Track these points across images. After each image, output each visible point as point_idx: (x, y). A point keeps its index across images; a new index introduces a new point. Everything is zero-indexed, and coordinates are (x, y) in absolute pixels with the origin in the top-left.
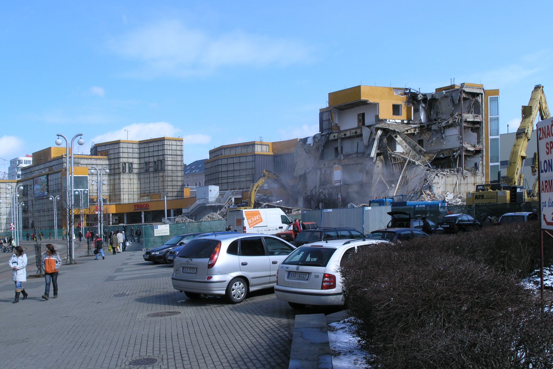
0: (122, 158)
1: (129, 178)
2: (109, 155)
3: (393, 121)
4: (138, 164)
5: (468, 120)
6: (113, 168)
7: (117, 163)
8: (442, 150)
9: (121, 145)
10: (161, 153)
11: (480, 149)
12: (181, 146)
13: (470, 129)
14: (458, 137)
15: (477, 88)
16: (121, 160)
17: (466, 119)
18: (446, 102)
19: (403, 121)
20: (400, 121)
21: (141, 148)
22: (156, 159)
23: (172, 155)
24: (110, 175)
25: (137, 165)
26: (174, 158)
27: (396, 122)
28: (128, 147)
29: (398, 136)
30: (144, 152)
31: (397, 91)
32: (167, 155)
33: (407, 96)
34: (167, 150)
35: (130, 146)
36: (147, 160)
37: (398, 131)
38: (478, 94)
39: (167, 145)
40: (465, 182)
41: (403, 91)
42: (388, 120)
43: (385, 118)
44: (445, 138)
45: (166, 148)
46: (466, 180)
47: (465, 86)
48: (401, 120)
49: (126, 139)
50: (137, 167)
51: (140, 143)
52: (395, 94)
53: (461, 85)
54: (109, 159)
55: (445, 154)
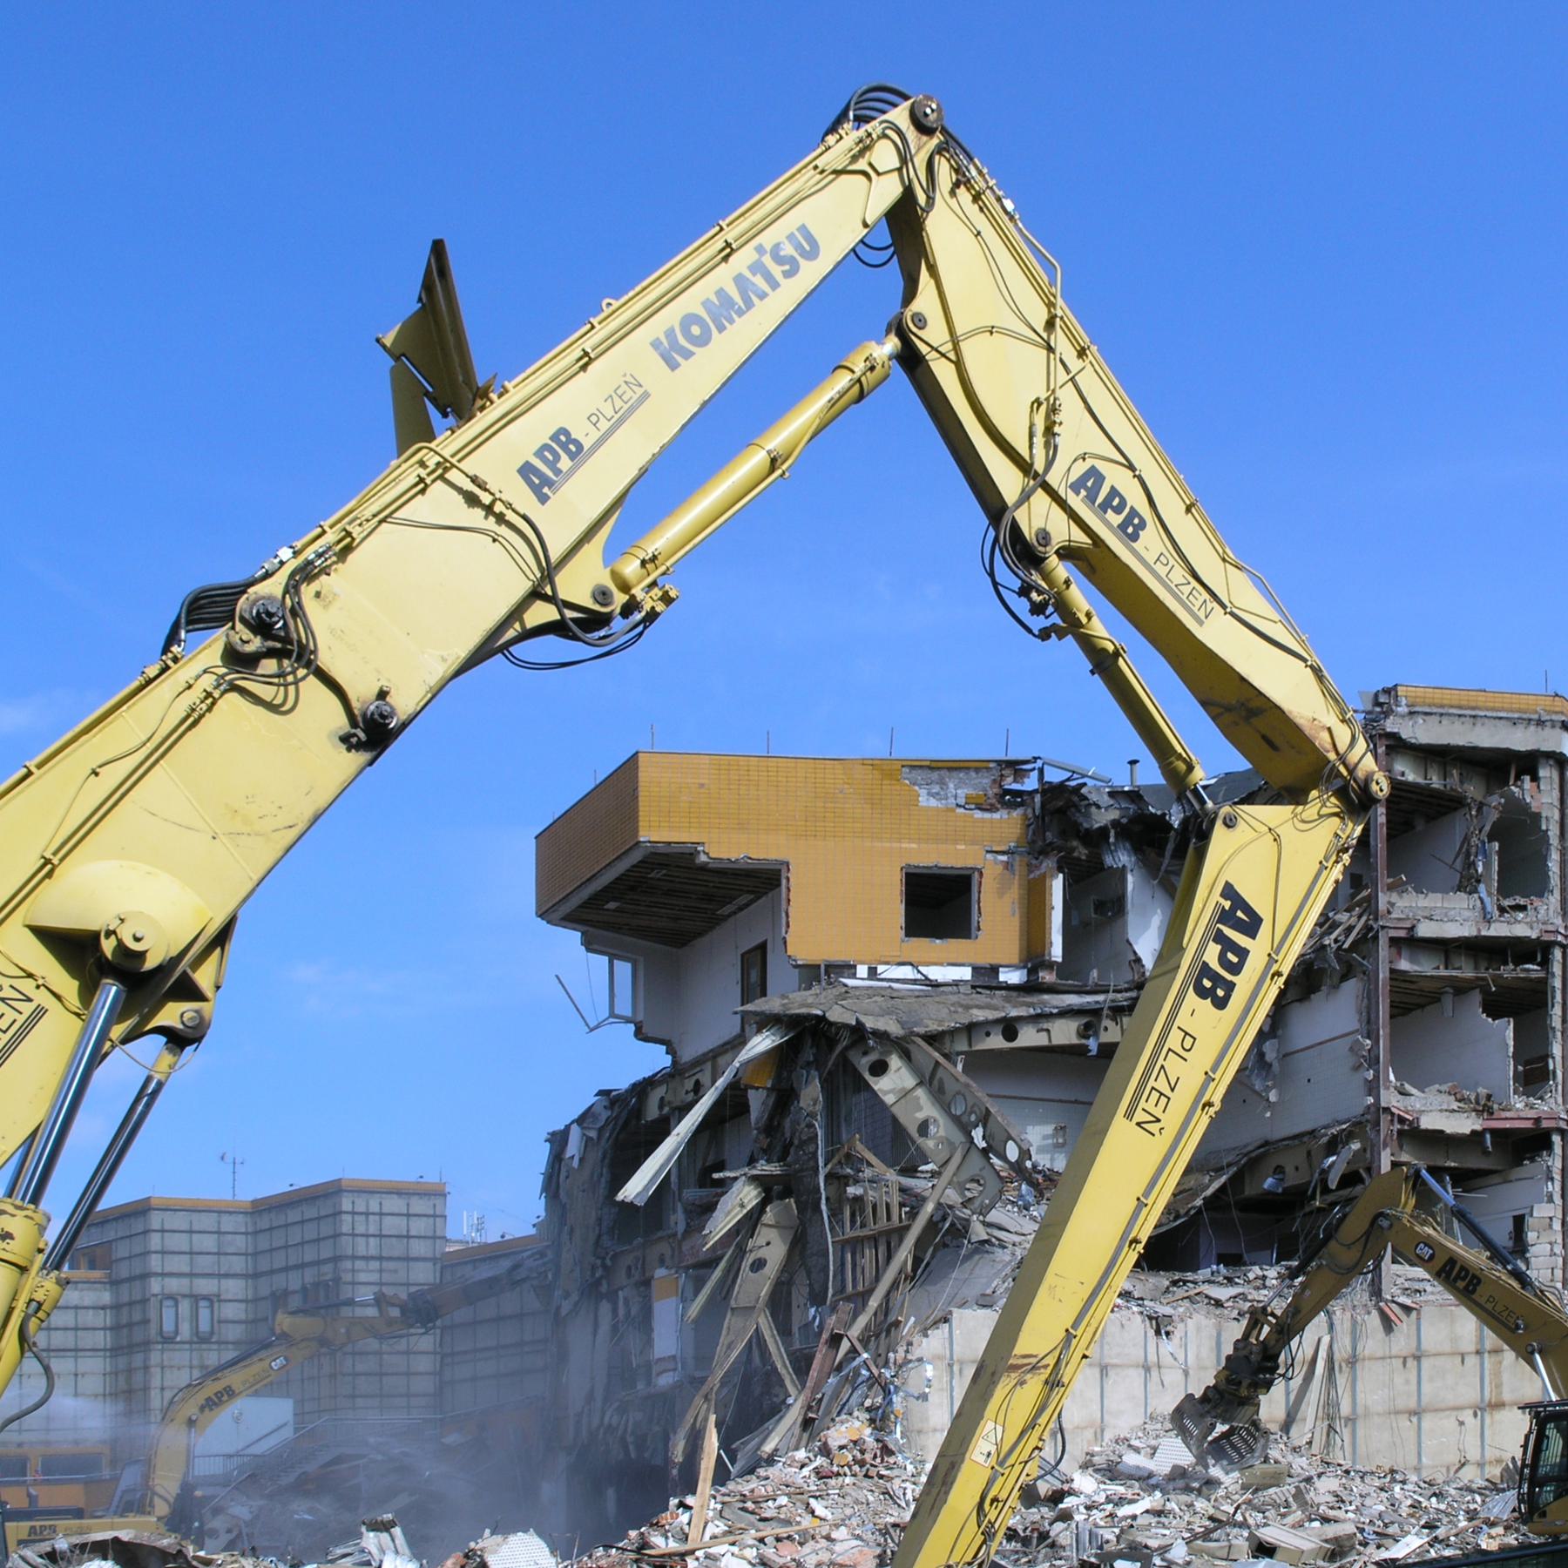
0: (156, 1274)
1: (195, 1362)
2: (114, 1266)
3: (907, 972)
4: (246, 1301)
5: (1425, 930)
6: (124, 1321)
7: (139, 1297)
8: (1268, 1147)
9: (156, 1220)
10: (326, 1251)
11: (1537, 1120)
12: (434, 1216)
13: (1476, 998)
14: (1351, 1049)
15: (1514, 722)
16: (155, 1286)
17: (1412, 928)
19: (994, 970)
20: (965, 973)
21: (261, 1231)
22: (310, 1275)
23: (380, 1258)
24: (115, 1351)
25: (243, 1306)
26: (396, 1271)
27: (928, 982)
28: (195, 1228)
29: (895, 1062)
30: (218, 1254)
31: (942, 783)
32: (354, 1258)
33: (1025, 814)
34: (354, 1235)
35: (207, 1221)
36: (279, 1281)
37: (894, 1029)
38: (1528, 763)
39: (353, 1213)
40: (1402, 1340)
42: (862, 971)
43: (838, 957)
44: (1276, 1067)
45: (346, 1228)
46: (1405, 1326)
47: (1403, 709)
48: (976, 970)
49: (229, 1197)
50: (243, 1316)
51: (262, 1207)
52: (924, 800)
53: (1377, 703)
54: (114, 1283)
55: (1289, 1169)
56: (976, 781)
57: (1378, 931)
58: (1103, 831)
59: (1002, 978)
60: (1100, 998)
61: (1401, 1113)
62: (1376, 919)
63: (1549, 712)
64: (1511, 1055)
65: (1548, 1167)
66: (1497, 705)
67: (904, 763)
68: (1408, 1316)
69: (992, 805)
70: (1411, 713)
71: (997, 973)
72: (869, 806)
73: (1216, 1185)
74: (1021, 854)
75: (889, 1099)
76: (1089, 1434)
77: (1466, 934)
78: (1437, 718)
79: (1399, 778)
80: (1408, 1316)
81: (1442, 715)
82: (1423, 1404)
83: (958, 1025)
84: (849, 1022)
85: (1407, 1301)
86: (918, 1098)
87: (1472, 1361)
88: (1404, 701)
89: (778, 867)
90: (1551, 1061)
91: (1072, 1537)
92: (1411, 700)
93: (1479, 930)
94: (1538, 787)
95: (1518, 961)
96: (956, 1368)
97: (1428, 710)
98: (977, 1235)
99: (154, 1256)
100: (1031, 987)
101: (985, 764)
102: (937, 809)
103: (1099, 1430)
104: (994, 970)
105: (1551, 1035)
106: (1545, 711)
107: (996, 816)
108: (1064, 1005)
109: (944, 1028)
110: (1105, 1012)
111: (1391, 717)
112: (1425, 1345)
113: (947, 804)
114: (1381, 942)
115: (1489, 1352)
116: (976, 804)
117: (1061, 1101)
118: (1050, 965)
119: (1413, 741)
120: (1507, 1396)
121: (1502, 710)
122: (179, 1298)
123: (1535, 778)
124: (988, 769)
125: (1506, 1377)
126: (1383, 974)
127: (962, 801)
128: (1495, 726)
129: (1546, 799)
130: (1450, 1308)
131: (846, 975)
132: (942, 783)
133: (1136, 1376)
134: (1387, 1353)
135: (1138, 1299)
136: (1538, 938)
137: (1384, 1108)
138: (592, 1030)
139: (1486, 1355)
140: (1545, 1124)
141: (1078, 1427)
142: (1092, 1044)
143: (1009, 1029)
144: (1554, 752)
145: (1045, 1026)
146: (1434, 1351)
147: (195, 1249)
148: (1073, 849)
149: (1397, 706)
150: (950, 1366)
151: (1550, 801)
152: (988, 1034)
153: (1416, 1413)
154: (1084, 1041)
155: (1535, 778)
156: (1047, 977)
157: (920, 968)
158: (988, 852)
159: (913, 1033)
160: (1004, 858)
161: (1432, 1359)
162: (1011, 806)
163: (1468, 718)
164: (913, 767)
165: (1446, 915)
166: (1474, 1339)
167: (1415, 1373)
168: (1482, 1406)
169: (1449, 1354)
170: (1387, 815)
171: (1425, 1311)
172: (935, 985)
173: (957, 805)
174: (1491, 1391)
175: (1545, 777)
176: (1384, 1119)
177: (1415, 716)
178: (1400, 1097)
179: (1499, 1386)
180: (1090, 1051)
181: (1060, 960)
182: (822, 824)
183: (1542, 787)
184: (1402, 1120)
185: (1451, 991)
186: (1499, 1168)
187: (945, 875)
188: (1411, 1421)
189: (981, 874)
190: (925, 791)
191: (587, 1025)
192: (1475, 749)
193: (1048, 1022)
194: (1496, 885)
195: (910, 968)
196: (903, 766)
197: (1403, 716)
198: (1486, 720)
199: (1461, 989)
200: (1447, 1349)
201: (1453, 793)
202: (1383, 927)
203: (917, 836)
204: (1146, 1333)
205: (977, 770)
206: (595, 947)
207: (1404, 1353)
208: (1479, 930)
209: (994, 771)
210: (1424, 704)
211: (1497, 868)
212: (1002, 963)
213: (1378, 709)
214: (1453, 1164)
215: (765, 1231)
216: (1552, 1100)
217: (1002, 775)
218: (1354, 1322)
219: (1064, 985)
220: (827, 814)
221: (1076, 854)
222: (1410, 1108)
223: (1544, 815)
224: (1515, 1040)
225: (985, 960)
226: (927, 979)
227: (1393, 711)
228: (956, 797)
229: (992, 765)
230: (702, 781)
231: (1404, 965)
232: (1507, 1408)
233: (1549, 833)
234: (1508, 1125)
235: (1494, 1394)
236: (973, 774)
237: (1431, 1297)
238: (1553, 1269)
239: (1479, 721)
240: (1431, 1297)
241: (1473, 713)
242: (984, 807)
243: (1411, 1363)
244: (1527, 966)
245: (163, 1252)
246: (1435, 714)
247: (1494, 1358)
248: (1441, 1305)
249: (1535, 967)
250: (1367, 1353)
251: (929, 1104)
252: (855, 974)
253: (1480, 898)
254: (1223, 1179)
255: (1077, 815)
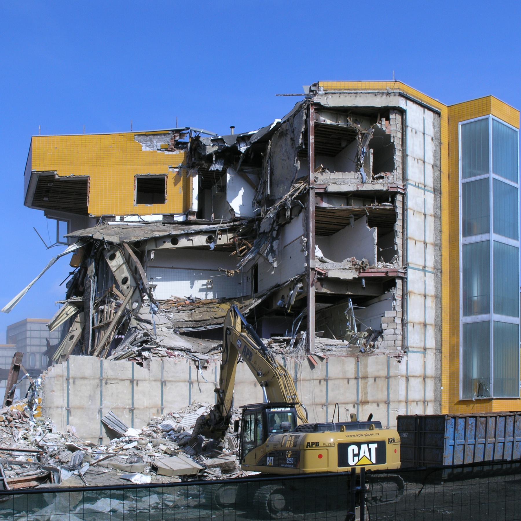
3: (136, 218)
5: (332, 189)
9: (29, 326)
17: (325, 189)
18: (284, 150)
19: (172, 216)
20: (160, 218)
29: (118, 254)
31: (151, 141)
37: (115, 240)
41: (168, 139)
42: (118, 218)
43: (107, 213)
46: (320, 365)
47: (322, 92)
48: (164, 216)
52: (145, 148)
56: (165, 139)
57: (309, 190)
58: (211, 155)
59: (175, 219)
60: (215, 226)
61: (320, 271)
62: (309, 185)
63: (392, 89)
64: (376, 243)
65: (393, 294)
66: (367, 87)
67: (136, 134)
68: (322, 361)
69: (172, 148)
70: (326, 94)
71: (173, 217)
72: (122, 152)
73: (256, 304)
74: (184, 168)
75: (114, 269)
76: (154, 411)
77: (352, 190)
78: (338, 95)
79: (323, 123)
80: (322, 361)
81: (340, 93)
82: (329, 401)
83: (145, 238)
84: (99, 238)
85: (321, 354)
86: (123, 269)
87: (353, 382)
88: (322, 89)
89: (86, 179)
90: (395, 246)
91: (72, 458)
92: (326, 88)
93: (358, 188)
94: (390, 123)
95: (380, 202)
96: (71, 381)
97: (333, 92)
98: (132, 325)
99: (28, 339)
100: (187, 223)
101: (167, 132)
102: (149, 151)
103: (160, 409)
104: (172, 216)
105: (395, 234)
106: (390, 88)
107: (174, 153)
108: (199, 229)
109: (138, 240)
110: (217, 232)
111: (316, 96)
112: (330, 375)
113: (153, 149)
114: (310, 195)
115: (361, 378)
116: (165, 149)
117: (211, 270)
118: (193, 213)
119: (327, 106)
120: (369, 398)
121: (370, 89)
122: (36, 354)
123: (388, 119)
124: (169, 134)
125: (369, 390)
126: (312, 209)
127: (159, 148)
128: (366, 97)
129: (393, 128)
130: (342, 358)
131: (111, 220)
132: (151, 141)
133: (184, 388)
134: (312, 378)
135: (193, 352)
136: (387, 190)
137: (311, 268)
138: (48, 248)
139: (360, 380)
140: (390, 274)
141: (147, 408)
142: (212, 246)
143: (175, 239)
144: (395, 107)
145: (191, 238)
146: (334, 377)
147: (41, 337)
148: (203, 164)
149: (319, 91)
150: (68, 380)
151: (395, 129)
152: (164, 242)
153: (325, 405)
154: (209, 244)
155: (388, 119)
156: (192, 218)
157: (141, 217)
158: (170, 168)
159: (123, 242)
160: (177, 170)
161: (333, 381)
162: (182, 148)
163: (353, 94)
164: (139, 135)
165: (343, 182)
166: (354, 372)
167: (325, 386)
168: (358, 402)
169: (341, 379)
170: (315, 139)
171: (331, 360)
172: (147, 223)
173: (158, 150)
174: (362, 396)
175: (393, 119)
176: (311, 273)
177: (327, 95)
178: (321, 263)
179: (366, 393)
180: (211, 248)
181: (196, 210)
182: (103, 160)
183: (391, 123)
184: (319, 273)
185: (353, 216)
186: (376, 295)
187: (158, 178)
188: (322, 408)
189: (167, 177)
190: (145, 145)
191: (46, 246)
192: (357, 107)
193: (192, 236)
194: (372, 168)
195: (137, 216)
196: (135, 135)
197: (322, 95)
198: (362, 94)
199: (358, 216)
200: (341, 376)
201: (351, 128)
202: (312, 188)
203: (141, 163)
204: (190, 367)
205: (164, 135)
206: (49, 216)
207: (320, 378)
208: (358, 188)
209: (171, 135)
210: (332, 89)
211: (372, 160)
212: (175, 213)
213: (312, 93)
214: (350, 293)
215: (76, 324)
216: (397, 264)
217: (175, 136)
218: (296, 364)
219: (201, 221)
220: (105, 156)
221: (203, 166)
222: (325, 268)
223: (392, 135)
224: (378, 237)
225: (168, 212)
226: (143, 221)
227: (317, 93)
228: (157, 146)
229: (170, 132)
230: (56, 146)
231: (324, 205)
232: (370, 404)
233: (395, 143)
234: (373, 275)
235: (363, 397)
236: (163, 136)
237: (334, 353)
238: (395, 341)
239: (358, 95)
240: (334, 353)
241: (355, 92)
242: (168, 149)
243: (323, 383)
244: (384, 203)
245: (31, 338)
246: (337, 93)
247: (364, 381)
248: (339, 357)
249: (389, 204)
250: (302, 377)
251: (127, 271)
252: (115, 220)
253: (361, 174)
254: (260, 301)
255: (201, 150)
